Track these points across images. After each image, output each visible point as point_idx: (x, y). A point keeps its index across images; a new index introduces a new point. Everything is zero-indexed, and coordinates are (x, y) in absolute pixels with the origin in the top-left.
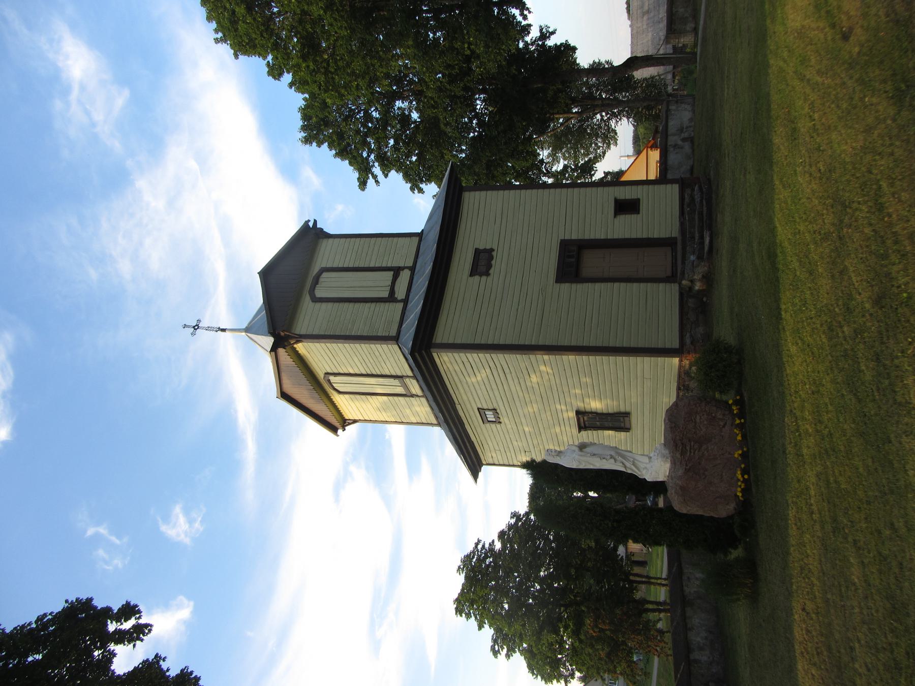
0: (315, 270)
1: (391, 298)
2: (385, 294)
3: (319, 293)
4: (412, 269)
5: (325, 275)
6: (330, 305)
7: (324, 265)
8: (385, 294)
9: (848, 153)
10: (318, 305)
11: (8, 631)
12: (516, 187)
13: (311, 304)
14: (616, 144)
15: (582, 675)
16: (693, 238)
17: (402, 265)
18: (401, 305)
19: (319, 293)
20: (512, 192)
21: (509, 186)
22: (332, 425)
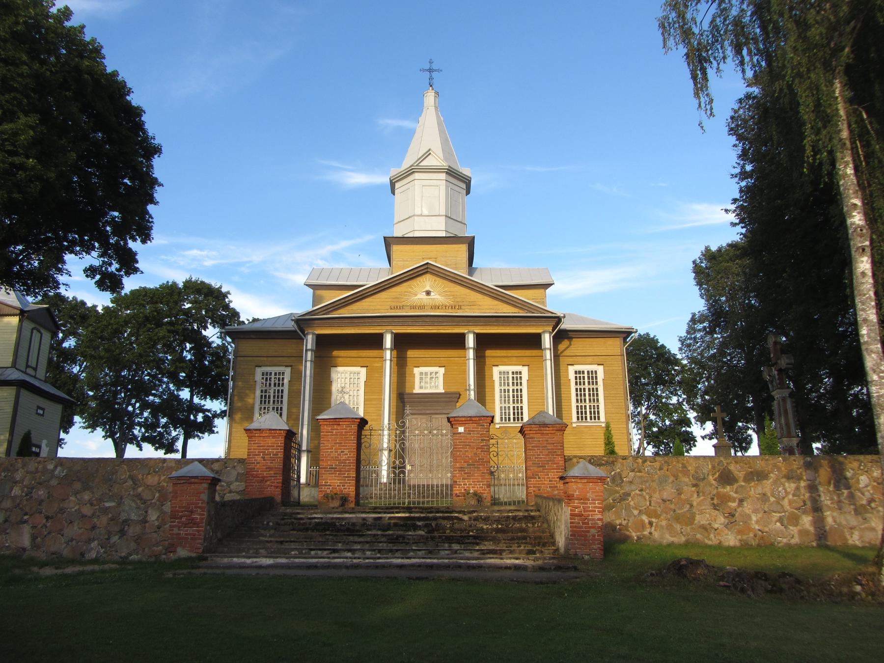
0: (43, 331)
1: (27, 366)
2: (29, 364)
3: (35, 331)
4: (35, 377)
5: (40, 335)
6: (29, 337)
7: (43, 335)
8: (29, 364)
9: (165, 372)
10: (30, 331)
11: (735, 235)
12: (46, 375)
13: (31, 328)
14: (145, 113)
15: (139, 240)
16: (374, 535)
17: (37, 372)
18: (24, 369)
19: (35, 331)
20: (45, 372)
21: (46, 373)
22: (14, 426)
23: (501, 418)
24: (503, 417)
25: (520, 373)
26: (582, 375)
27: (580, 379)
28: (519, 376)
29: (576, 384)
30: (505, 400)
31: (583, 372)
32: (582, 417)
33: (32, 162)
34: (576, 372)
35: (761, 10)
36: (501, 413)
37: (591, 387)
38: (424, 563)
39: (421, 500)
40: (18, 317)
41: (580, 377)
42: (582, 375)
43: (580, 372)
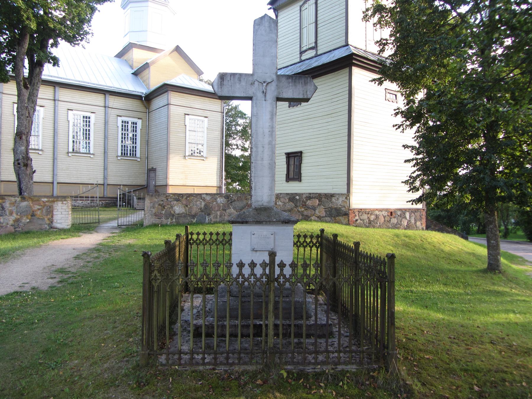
23: (122, 153)
24: (123, 152)
25: (89, 118)
26: (126, 124)
27: (125, 127)
28: (88, 120)
29: (122, 129)
30: (86, 137)
31: (128, 122)
32: (133, 154)
33: (420, 62)
34: (122, 122)
35: (396, 1)
36: (122, 150)
37: (126, 132)
38: (385, 319)
39: (86, 216)
40: (43, 77)
41: (125, 125)
42: (126, 124)
43: (125, 122)
